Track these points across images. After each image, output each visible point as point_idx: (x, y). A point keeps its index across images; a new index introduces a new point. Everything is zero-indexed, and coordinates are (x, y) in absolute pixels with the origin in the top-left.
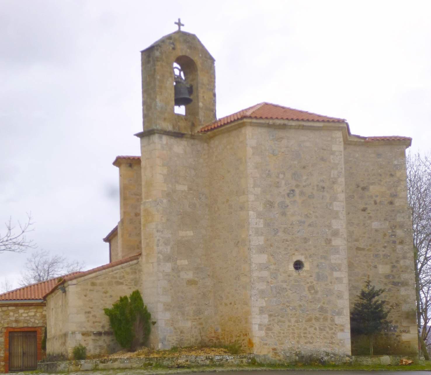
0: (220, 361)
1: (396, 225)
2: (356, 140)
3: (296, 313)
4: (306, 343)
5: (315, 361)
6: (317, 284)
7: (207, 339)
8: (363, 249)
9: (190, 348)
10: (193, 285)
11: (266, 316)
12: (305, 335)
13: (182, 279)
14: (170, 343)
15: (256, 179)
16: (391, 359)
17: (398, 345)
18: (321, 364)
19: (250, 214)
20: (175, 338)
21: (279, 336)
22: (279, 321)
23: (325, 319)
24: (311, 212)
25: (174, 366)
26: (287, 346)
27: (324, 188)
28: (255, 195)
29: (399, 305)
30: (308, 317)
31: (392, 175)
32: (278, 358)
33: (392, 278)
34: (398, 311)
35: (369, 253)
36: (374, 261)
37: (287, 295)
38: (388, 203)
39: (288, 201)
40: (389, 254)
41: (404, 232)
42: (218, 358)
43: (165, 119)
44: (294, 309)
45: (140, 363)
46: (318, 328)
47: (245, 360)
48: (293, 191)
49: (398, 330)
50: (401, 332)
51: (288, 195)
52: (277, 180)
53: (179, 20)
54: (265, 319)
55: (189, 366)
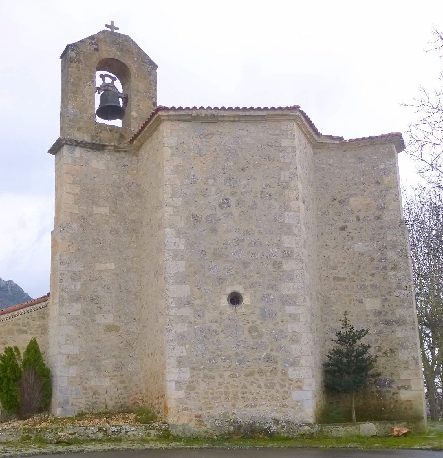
0: (117, 433)
1: (386, 246)
2: (328, 141)
3: (231, 365)
4: (246, 407)
5: (259, 432)
6: (262, 323)
7: (131, 402)
8: (344, 279)
9: (108, 414)
10: (114, 332)
11: (187, 370)
12: (244, 396)
13: (98, 324)
14: (75, 407)
15: (176, 186)
16: (377, 428)
17: (395, 406)
18: (268, 437)
19: (166, 233)
20: (84, 401)
21: (205, 398)
22: (206, 376)
23: (274, 372)
24: (253, 227)
25: (53, 441)
26: (217, 412)
27: (270, 195)
28: (174, 207)
29: (394, 352)
30: (248, 370)
31: (378, 183)
32: (204, 428)
33: (383, 316)
34: (393, 360)
35: (352, 284)
36: (358, 294)
37: (217, 340)
38: (375, 218)
39: (219, 214)
40: (378, 284)
41: (397, 254)
42: (114, 429)
43: (79, 129)
44: (228, 359)
45: (16, 436)
46: (263, 385)
47: (153, 432)
48: (227, 200)
49: (394, 386)
50: (399, 388)
51: (220, 205)
52: (205, 187)
53: (112, 22)
54: (186, 374)
55: (70, 442)
